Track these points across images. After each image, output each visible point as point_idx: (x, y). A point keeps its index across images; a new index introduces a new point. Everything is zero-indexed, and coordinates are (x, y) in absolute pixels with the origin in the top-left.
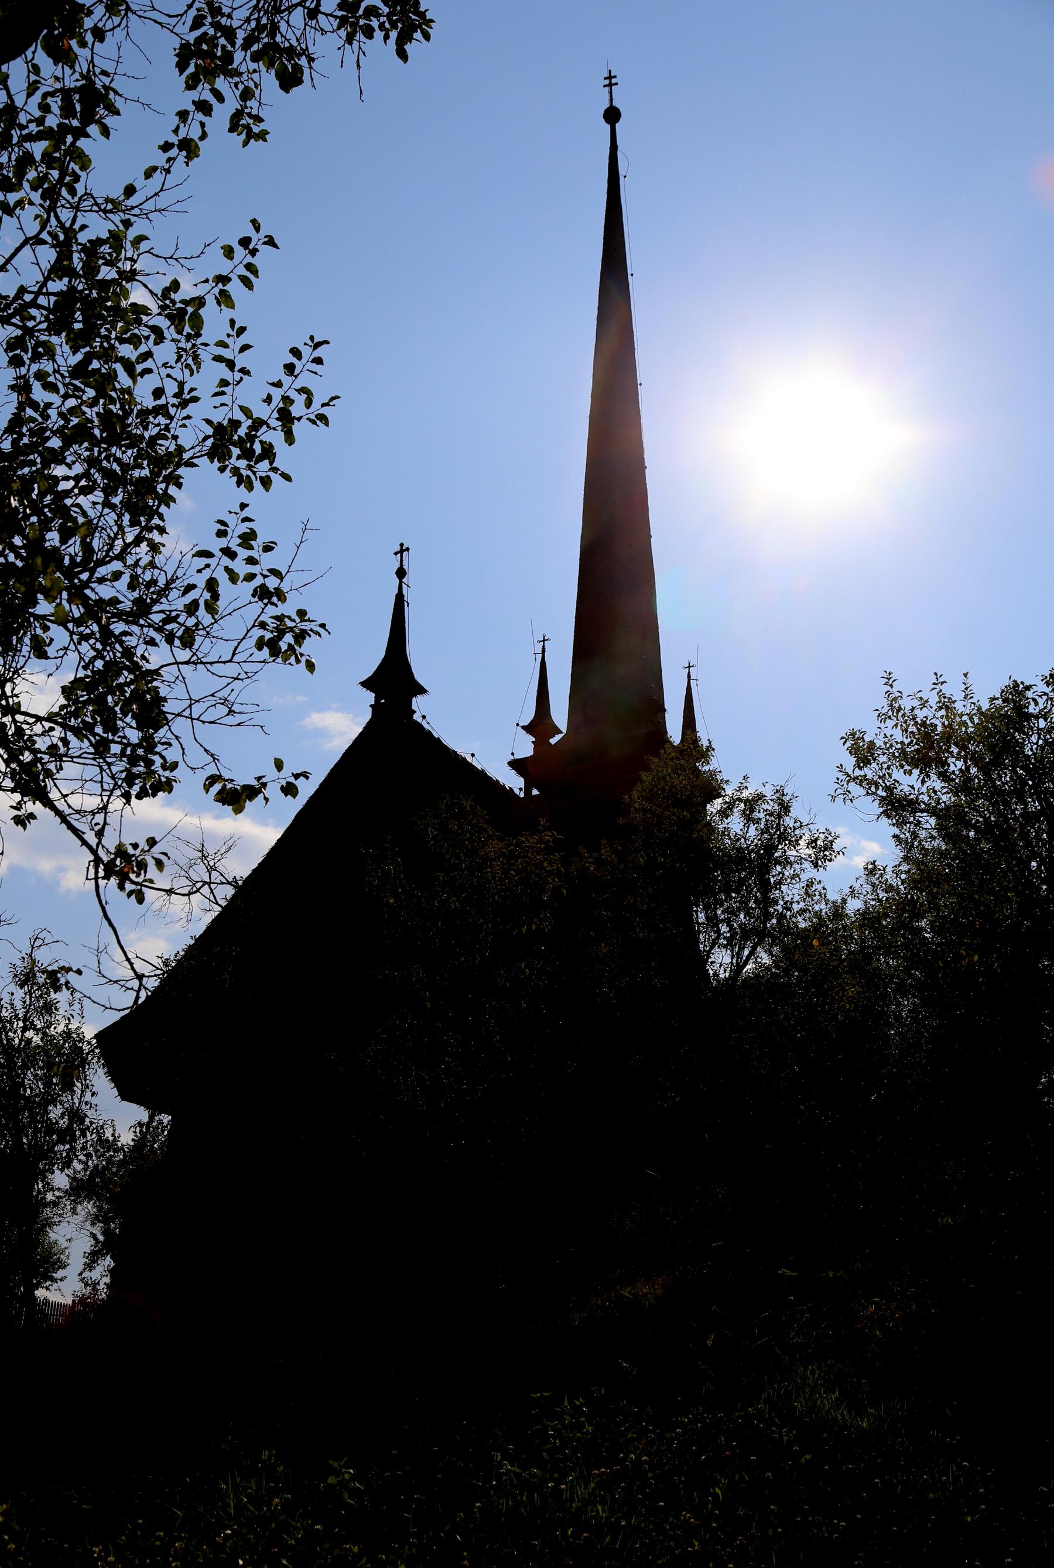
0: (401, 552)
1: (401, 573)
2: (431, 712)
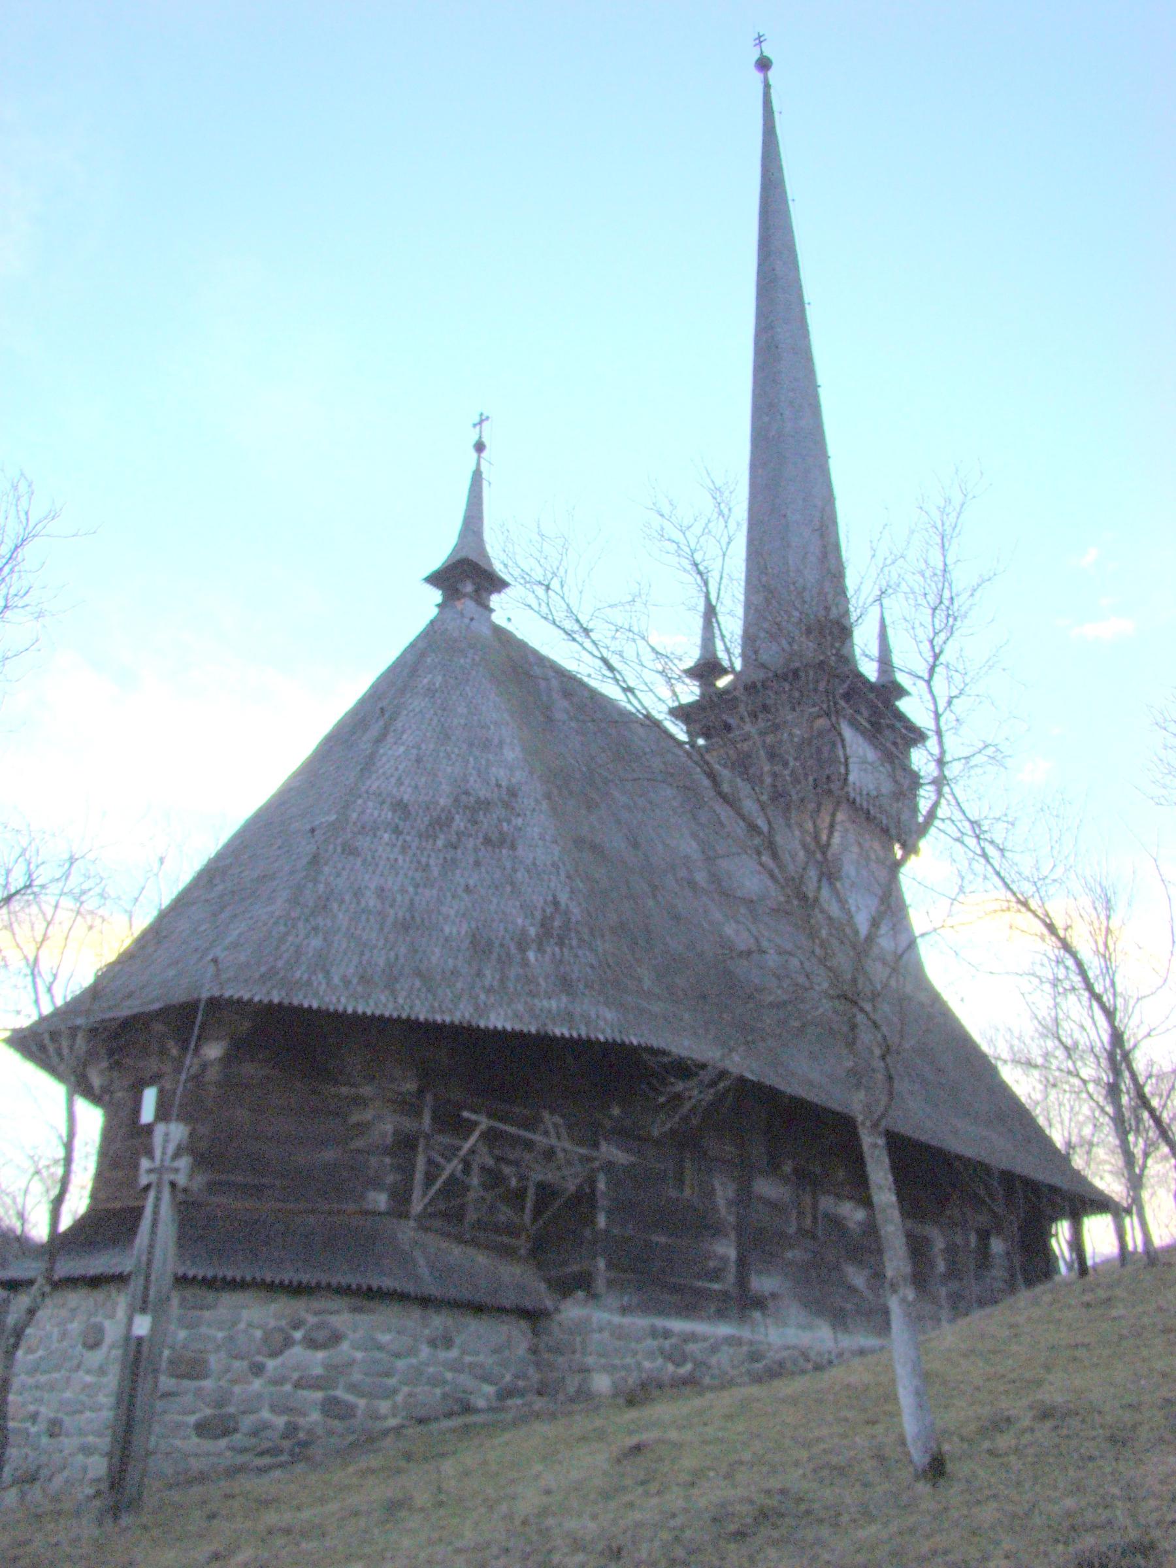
0: (481, 423)
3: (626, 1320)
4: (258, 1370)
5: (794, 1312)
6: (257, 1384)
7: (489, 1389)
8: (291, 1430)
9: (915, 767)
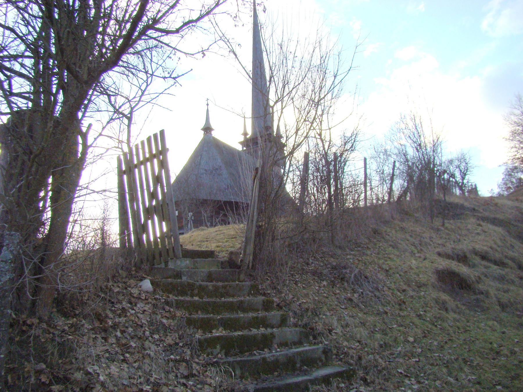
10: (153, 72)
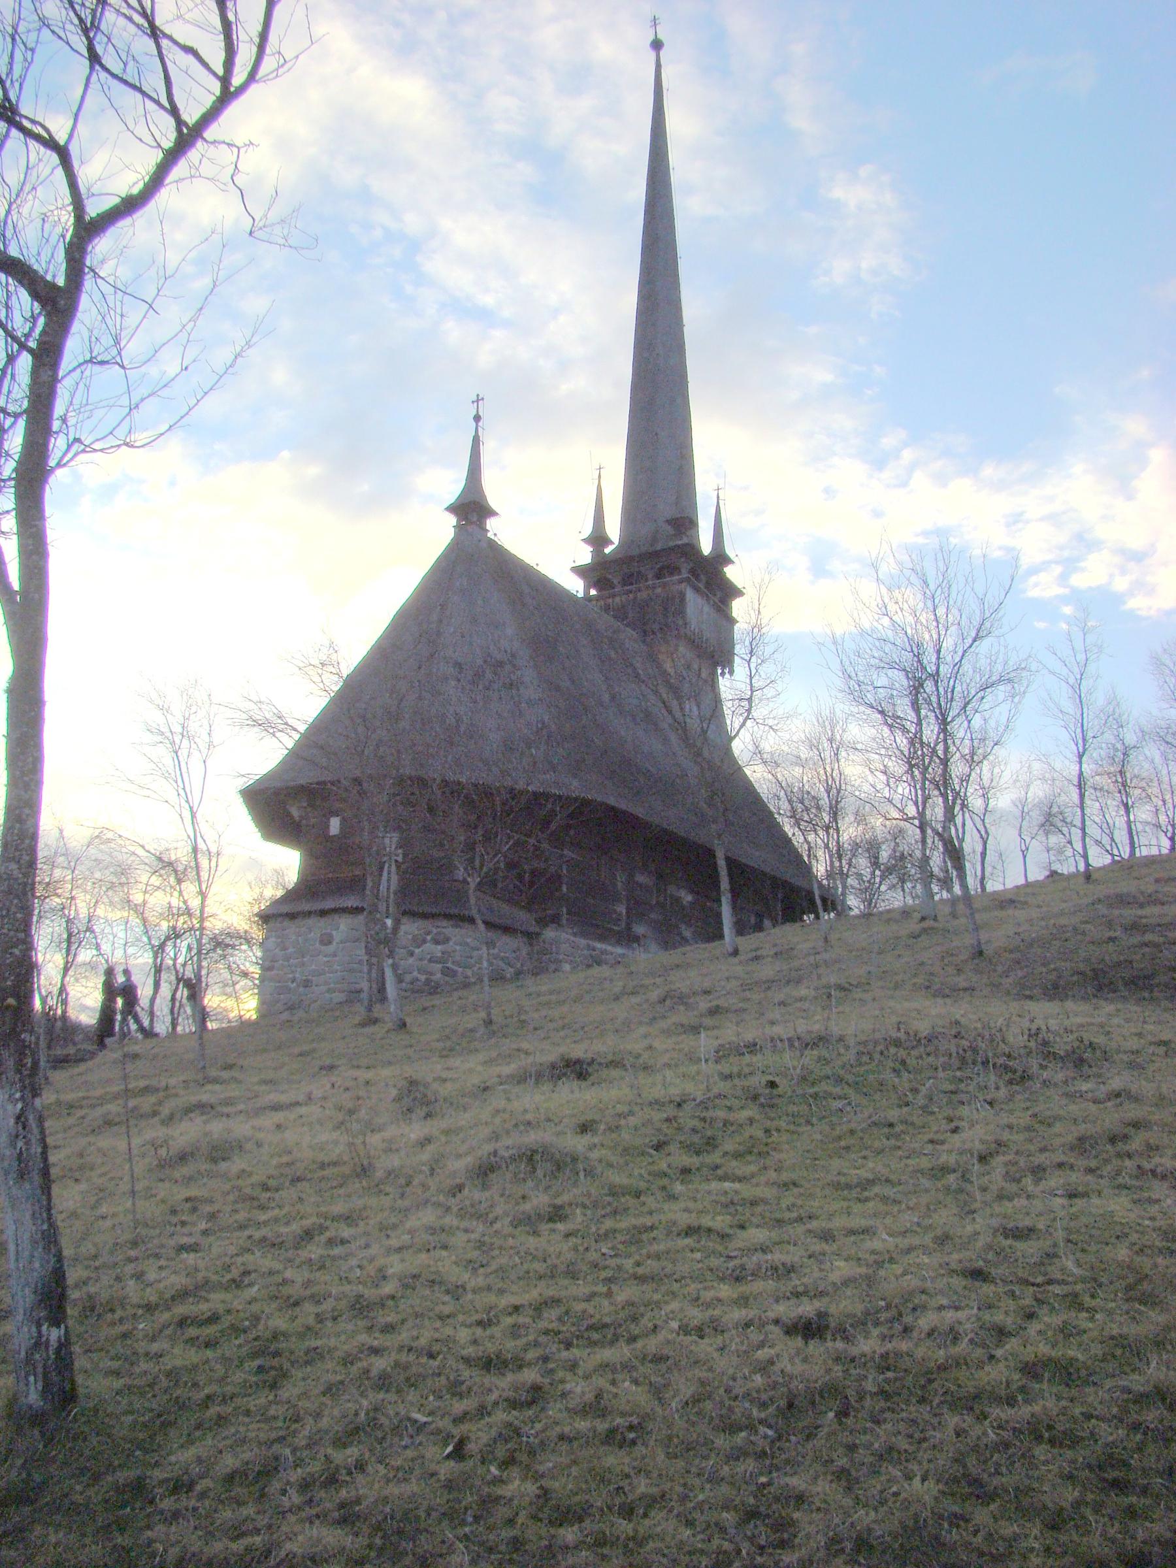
0: (478, 401)
1: (477, 418)
2: (507, 531)
3: (577, 940)
4: (412, 954)
5: (653, 947)
6: (411, 960)
7: (512, 970)
8: (428, 982)
9: (734, 614)
10: (39, 30)
